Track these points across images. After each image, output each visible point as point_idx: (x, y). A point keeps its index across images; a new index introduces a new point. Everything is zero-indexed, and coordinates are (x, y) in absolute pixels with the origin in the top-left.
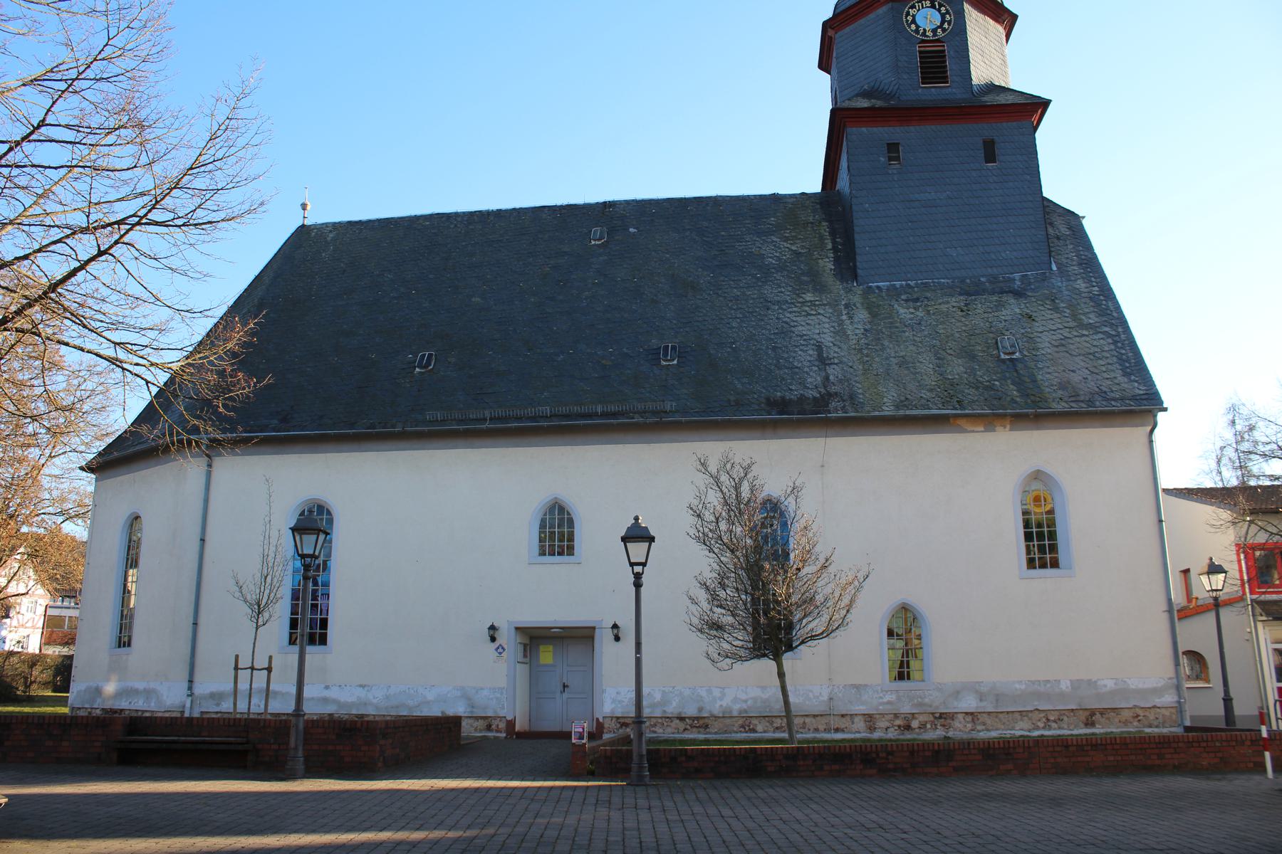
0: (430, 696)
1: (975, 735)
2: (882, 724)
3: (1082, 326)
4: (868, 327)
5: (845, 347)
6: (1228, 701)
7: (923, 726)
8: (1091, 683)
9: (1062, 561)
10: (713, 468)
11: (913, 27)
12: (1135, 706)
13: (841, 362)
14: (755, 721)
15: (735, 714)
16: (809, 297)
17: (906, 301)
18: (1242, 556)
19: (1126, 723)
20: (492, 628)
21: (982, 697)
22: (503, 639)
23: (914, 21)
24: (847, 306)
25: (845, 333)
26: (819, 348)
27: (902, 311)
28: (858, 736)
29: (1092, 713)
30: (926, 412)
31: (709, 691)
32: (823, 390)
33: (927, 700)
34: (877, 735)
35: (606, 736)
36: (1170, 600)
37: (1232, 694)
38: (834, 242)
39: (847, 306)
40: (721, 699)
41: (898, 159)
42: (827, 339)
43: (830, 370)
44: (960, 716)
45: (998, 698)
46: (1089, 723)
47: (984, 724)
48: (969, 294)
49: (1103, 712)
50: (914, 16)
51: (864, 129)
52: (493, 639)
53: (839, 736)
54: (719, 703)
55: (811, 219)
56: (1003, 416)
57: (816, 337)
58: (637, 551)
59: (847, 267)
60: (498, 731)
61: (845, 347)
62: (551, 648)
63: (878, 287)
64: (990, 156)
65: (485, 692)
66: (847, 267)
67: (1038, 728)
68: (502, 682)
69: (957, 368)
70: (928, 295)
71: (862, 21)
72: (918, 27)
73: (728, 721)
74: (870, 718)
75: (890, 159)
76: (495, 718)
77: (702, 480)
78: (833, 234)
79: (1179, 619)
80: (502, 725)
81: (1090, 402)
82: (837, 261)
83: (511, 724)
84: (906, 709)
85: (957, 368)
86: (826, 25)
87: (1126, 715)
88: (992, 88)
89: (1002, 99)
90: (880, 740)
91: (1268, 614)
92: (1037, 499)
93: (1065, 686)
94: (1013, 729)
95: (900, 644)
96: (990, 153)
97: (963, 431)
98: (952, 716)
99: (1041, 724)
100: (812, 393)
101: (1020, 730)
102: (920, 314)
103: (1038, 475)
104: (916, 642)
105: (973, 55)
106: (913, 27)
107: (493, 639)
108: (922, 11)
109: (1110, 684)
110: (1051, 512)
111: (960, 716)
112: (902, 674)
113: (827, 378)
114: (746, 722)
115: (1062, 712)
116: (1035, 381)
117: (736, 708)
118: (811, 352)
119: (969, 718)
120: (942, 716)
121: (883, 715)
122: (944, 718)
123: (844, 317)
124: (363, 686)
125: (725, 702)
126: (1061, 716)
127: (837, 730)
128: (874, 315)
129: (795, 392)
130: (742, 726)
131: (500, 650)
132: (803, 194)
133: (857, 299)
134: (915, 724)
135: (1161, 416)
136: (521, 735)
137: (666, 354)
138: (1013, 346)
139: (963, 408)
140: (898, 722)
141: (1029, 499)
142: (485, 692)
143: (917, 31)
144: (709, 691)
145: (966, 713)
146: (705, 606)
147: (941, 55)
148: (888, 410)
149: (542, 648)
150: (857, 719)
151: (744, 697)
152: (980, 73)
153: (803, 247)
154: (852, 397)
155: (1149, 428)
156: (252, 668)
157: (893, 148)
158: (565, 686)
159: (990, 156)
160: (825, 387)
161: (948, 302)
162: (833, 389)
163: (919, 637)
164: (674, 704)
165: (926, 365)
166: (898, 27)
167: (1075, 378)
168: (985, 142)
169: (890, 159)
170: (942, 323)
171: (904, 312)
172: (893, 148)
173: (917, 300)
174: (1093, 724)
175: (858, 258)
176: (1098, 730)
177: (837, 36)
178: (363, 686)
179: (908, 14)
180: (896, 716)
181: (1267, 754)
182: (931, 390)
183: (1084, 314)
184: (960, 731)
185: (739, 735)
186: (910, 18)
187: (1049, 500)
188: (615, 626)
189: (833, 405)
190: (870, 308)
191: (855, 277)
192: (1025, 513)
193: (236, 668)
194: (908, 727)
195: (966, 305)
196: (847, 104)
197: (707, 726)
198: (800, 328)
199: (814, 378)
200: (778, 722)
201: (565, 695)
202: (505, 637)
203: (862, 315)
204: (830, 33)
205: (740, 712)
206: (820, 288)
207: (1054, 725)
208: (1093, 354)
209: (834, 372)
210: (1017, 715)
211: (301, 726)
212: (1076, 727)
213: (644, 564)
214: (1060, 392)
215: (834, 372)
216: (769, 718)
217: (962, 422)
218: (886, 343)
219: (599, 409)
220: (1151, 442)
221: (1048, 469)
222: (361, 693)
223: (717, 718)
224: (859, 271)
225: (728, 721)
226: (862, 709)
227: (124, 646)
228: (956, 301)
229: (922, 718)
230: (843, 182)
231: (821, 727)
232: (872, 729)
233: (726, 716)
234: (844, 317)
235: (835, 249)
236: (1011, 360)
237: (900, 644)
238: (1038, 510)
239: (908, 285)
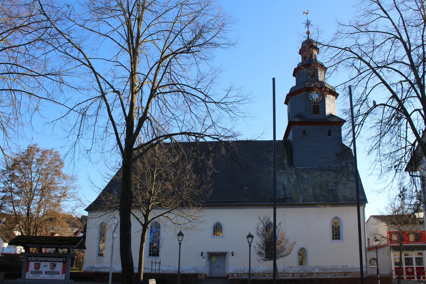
0: (186, 269)
1: (318, 278)
2: (296, 275)
3: (350, 180)
4: (296, 179)
5: (290, 185)
6: (378, 270)
7: (306, 276)
8: (346, 266)
9: (341, 238)
10: (261, 219)
11: (311, 99)
12: (356, 272)
13: (289, 189)
14: (266, 275)
15: (261, 273)
16: (281, 171)
17: (306, 172)
18: (388, 235)
19: (354, 275)
20: (202, 253)
21: (320, 269)
22: (204, 255)
23: (312, 97)
24: (291, 174)
25: (290, 181)
26: (284, 185)
27: (304, 175)
28: (290, 278)
29: (346, 273)
30: (310, 203)
31: (255, 267)
32: (284, 196)
33: (307, 270)
34: (295, 278)
35: (230, 278)
36: (366, 247)
37: (379, 269)
38: (287, 155)
39: (291, 174)
40: (258, 269)
41: (305, 134)
42: (286, 183)
43: (286, 191)
44: (315, 274)
45: (324, 269)
46: (345, 275)
47: (320, 275)
48: (322, 171)
49: (348, 273)
50: (312, 96)
51: (297, 127)
52: (202, 255)
53: (286, 278)
54: (257, 270)
55: (281, 148)
56: (329, 204)
57: (283, 182)
58: (250, 239)
59: (291, 163)
60: (203, 277)
61: (290, 185)
62: (215, 257)
63: (299, 169)
64: (329, 134)
65: (200, 268)
66: (291, 163)
67: (333, 276)
68: (204, 265)
69: (318, 191)
70: (312, 171)
71: (298, 95)
72: (312, 99)
73: (259, 274)
74: (293, 274)
75: (304, 134)
76: (202, 274)
77: (259, 221)
78: (287, 153)
79: (368, 251)
80: (204, 275)
81: (350, 201)
82: (288, 161)
83: (206, 275)
84: (302, 272)
85: (318, 191)
86: (287, 95)
87: (354, 273)
88: (331, 116)
89: (334, 120)
90: (295, 279)
91: (393, 249)
92: (336, 223)
93: (340, 267)
94: (327, 276)
95: (301, 257)
96: (329, 134)
97: (319, 207)
98: (313, 273)
99: (334, 276)
100: (282, 197)
101: (329, 277)
102: (309, 176)
103: (336, 218)
104: (305, 256)
105: (327, 107)
106: (311, 99)
107: (202, 255)
108: (314, 94)
109: (350, 266)
110: (339, 226)
111: (315, 274)
112: (301, 263)
113: (285, 193)
114: (264, 274)
115: (339, 273)
116: (337, 195)
117: (261, 271)
118: (281, 186)
119: (317, 274)
120: (310, 273)
121: (296, 273)
122: (311, 274)
123: (290, 177)
124: (169, 266)
125: (259, 270)
126: (339, 273)
127: (285, 277)
128: (297, 176)
129: (277, 197)
130: (263, 276)
131: (204, 258)
132: (279, 140)
133: (293, 172)
134: (304, 275)
135: (366, 204)
136: (208, 278)
137: (245, 186)
138: (332, 186)
139: (319, 202)
140: (300, 275)
141: (334, 223)
142: (200, 268)
143: (312, 100)
144: (255, 267)
145: (316, 273)
146: (258, 249)
147: (318, 107)
148: (301, 202)
149: (213, 257)
150: (290, 274)
151: (263, 269)
152: (328, 112)
153: (279, 157)
154: (292, 198)
155: (364, 207)
156: (156, 263)
157: (304, 132)
158: (218, 266)
159: (329, 134)
160: (285, 195)
161: (316, 173)
162: (287, 196)
163: (306, 255)
164: (246, 270)
165: (310, 190)
166: (307, 98)
167: (347, 194)
168: (328, 131)
169: (304, 134)
170: (315, 179)
171: (305, 176)
172: (304, 132)
173: (309, 172)
174: (346, 276)
175: (294, 161)
176: (347, 277)
177: (291, 98)
178: (169, 266)
179: (310, 95)
180: (299, 273)
181: (379, 281)
182: (311, 197)
183: (351, 177)
184: (314, 276)
185: (262, 278)
186: (311, 96)
187: (339, 223)
188: (232, 252)
189: (287, 200)
190: (297, 174)
191: (293, 166)
192: (333, 226)
193: (152, 263)
194: (302, 276)
195: (321, 174)
196: (293, 120)
197: (254, 276)
198: (279, 180)
199: (282, 193)
200: (271, 275)
201: (218, 268)
202: (205, 255)
203: (295, 176)
204: (289, 97)
205: (262, 272)
206: (284, 169)
207: (337, 276)
208: (352, 188)
209: (287, 192)
210: (328, 274)
211: (180, 275)
212: (342, 276)
213: (251, 242)
214: (343, 198)
215: (287, 192)
216: (269, 274)
217: (319, 205)
218: (300, 184)
219: (229, 201)
220: (364, 210)
221: (339, 217)
222: (168, 268)
223: (257, 274)
224: (294, 164)
225: (259, 274)
226: (291, 272)
227: (101, 256)
228: (318, 173)
229: (306, 274)
230: (290, 138)
231: (281, 276)
232: (293, 276)
233: (259, 273)
234: (290, 177)
235: (288, 157)
236: (331, 189)
237: (301, 257)
238: (336, 226)
239: (306, 168)
